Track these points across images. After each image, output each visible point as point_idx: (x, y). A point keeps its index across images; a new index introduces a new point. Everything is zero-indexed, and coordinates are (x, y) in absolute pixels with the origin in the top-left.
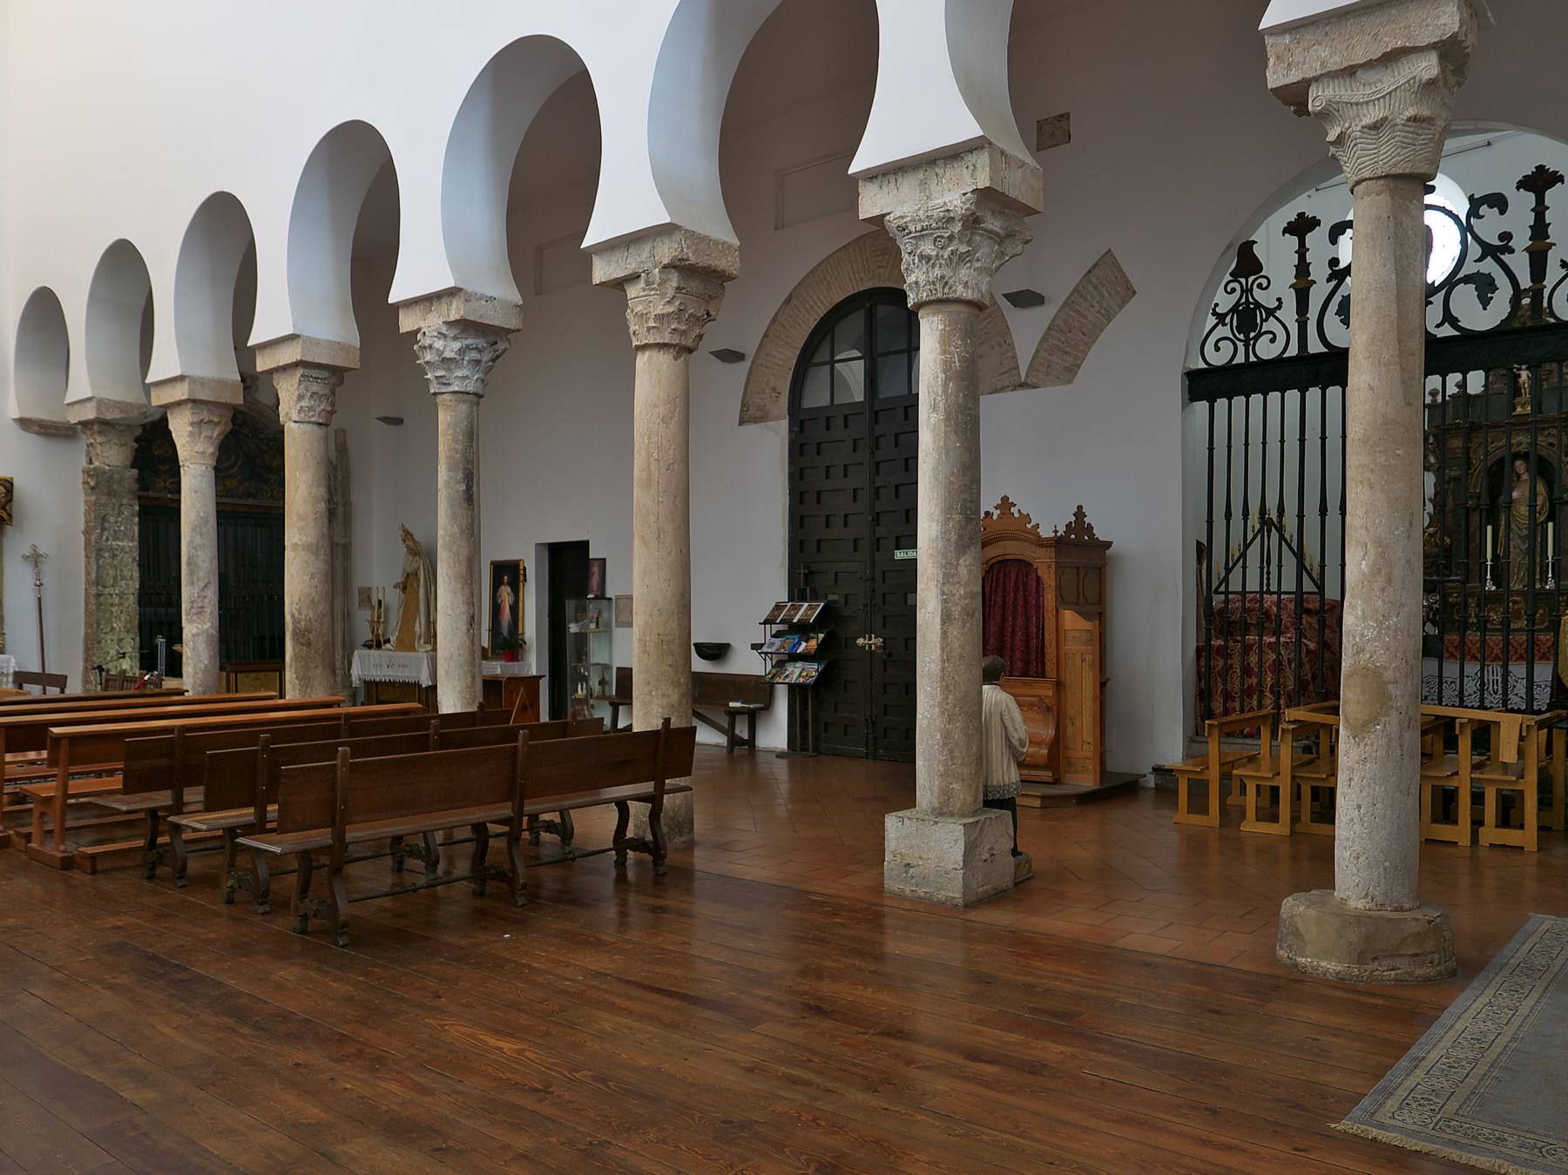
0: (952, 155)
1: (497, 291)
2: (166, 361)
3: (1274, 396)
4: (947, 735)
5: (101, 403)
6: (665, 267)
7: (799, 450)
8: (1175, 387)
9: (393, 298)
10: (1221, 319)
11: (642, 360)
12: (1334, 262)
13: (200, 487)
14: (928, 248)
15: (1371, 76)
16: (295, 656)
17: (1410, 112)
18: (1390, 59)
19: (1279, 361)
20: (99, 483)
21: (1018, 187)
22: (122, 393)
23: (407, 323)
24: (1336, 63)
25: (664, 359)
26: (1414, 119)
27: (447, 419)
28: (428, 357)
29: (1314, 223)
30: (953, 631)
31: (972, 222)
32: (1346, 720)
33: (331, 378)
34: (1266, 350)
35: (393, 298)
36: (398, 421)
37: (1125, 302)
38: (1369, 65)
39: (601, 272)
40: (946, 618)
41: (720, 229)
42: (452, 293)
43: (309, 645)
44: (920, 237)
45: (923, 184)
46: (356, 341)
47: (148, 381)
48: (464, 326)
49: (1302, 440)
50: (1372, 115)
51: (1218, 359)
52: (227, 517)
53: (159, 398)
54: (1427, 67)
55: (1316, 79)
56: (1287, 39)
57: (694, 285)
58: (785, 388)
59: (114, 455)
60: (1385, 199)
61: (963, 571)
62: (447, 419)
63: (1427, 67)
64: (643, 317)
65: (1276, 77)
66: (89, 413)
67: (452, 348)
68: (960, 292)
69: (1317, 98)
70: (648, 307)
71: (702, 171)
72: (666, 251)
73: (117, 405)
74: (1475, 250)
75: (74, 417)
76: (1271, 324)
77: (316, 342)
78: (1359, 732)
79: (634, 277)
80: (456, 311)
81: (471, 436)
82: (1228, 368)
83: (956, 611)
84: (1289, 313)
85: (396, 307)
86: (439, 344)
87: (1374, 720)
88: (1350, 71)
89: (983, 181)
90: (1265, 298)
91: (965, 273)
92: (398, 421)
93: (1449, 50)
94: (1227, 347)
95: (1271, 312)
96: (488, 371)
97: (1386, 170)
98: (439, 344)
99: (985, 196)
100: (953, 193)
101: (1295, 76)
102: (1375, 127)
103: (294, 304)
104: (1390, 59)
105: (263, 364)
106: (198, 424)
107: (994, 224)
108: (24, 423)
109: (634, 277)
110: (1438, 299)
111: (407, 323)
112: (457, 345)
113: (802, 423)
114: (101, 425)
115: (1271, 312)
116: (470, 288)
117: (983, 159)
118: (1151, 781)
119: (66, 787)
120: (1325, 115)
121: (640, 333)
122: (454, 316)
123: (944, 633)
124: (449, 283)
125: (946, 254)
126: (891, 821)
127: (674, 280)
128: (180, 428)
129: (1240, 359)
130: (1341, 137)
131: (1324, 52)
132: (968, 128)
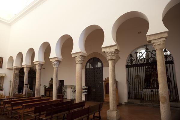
0: (113, 46)
1: (60, 57)
2: (24, 63)
3: (135, 68)
4: (113, 103)
5: (16, 67)
6: (80, 56)
7: (86, 72)
8: (125, 67)
9: (50, 58)
10: (129, 61)
11: (77, 64)
12: (139, 56)
13: (26, 76)
14: (110, 54)
15: (158, 40)
16: (36, 92)
17: (163, 43)
18: (160, 38)
19: (135, 65)
20: (15, 74)
21: (119, 49)
22: (19, 66)
23: (51, 60)
24: (154, 39)
25: (80, 64)
26: (163, 44)
27: (55, 69)
28: (53, 63)
29: (137, 52)
30: (114, 92)
31: (115, 52)
32: (161, 102)
33: (41, 65)
34: (134, 63)
35: (50, 58)
36: (44, 69)
37: (119, 59)
38: (158, 39)
39: (73, 56)
40: (113, 90)
41: (85, 52)
42: (56, 58)
43: (38, 91)
44: (109, 53)
45: (109, 48)
46: (44, 62)
47: (22, 65)
48: (57, 61)
49: (138, 72)
50: (159, 43)
51: (129, 64)
52: (29, 77)
53: (23, 67)
54: (164, 39)
55: (152, 40)
56: (149, 36)
57: (83, 57)
58: (85, 66)
59: (17, 72)
60: (160, 51)
61: (115, 86)
62: (55, 69)
63: (164, 39)
64: (77, 60)
65: (148, 40)
66: (15, 68)
67: (56, 63)
68: (113, 59)
69: (152, 42)
70: (78, 59)
71: (83, 47)
72: (80, 54)
73: (18, 67)
74: (153, 55)
75: (13, 68)
76: (134, 61)
77: (40, 62)
78: (163, 103)
79: (77, 56)
80: (56, 59)
81: (57, 71)
82: (130, 65)
83: (114, 90)
84: (136, 60)
85: (50, 59)
86: (54, 62)
87: (165, 102)
88: (156, 39)
89: (116, 48)
90: (133, 59)
91: (114, 57)
92: (44, 69)
93: (166, 38)
94: (130, 63)
95: (134, 60)
96: (59, 65)
97: (160, 48)
98: (54, 62)
99: (116, 50)
100: (113, 49)
101: (150, 40)
102: (159, 44)
103: (38, 58)
104: (160, 38)
105: (35, 64)
106: (27, 69)
107: (116, 52)
108: (8, 69)
109: (77, 56)
110: (150, 59)
111: (51, 60)
112: (56, 62)
113: (86, 69)
114: (16, 69)
115: (134, 60)
116: (58, 57)
117: (116, 46)
118: (124, 104)
119: (12, 108)
120: (153, 43)
121: (77, 62)
122: (56, 60)
123: (113, 92)
124: (56, 57)
125: (112, 55)
126: (107, 112)
127: (81, 57)
128: (25, 69)
129: (131, 64)
130: (155, 46)
131: (153, 38)
132: (115, 43)
